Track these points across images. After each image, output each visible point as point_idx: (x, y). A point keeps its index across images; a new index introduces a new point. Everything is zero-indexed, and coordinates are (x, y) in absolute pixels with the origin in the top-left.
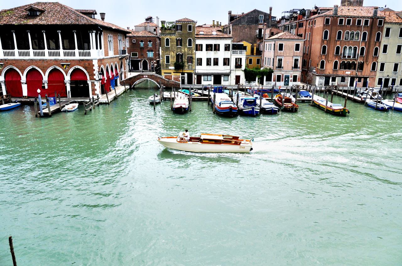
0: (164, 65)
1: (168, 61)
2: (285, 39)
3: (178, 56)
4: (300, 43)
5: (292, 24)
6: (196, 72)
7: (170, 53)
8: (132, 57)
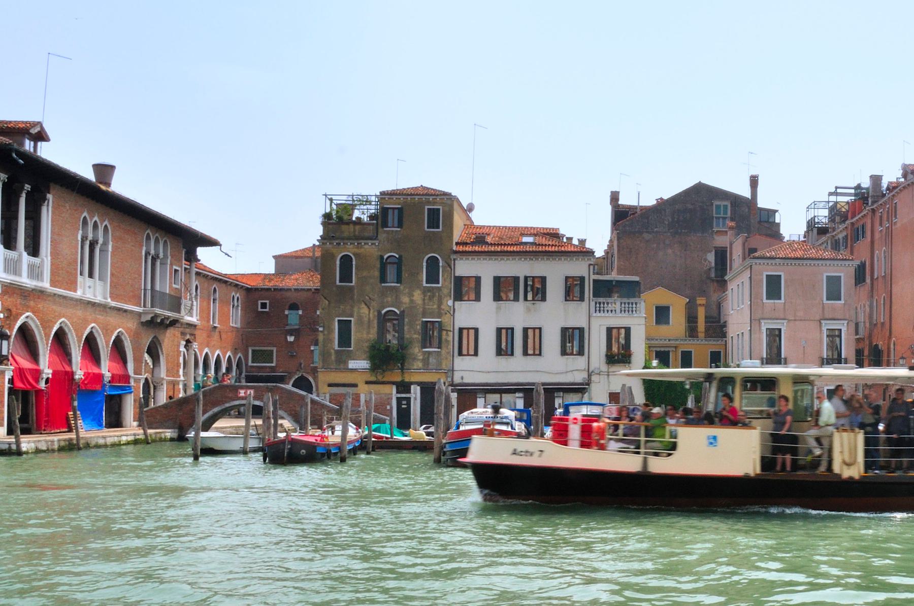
0: (330, 355)
1: (345, 338)
2: (785, 258)
3: (383, 320)
4: (842, 275)
5: (837, 238)
6: (457, 380)
7: (356, 309)
8: (250, 364)
